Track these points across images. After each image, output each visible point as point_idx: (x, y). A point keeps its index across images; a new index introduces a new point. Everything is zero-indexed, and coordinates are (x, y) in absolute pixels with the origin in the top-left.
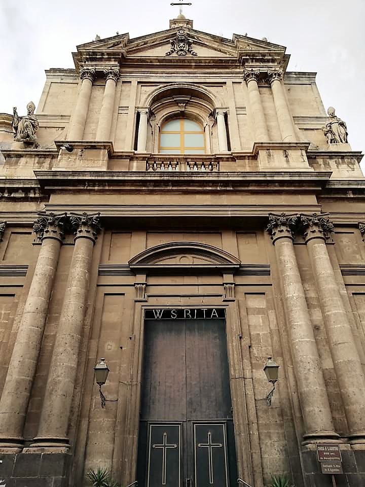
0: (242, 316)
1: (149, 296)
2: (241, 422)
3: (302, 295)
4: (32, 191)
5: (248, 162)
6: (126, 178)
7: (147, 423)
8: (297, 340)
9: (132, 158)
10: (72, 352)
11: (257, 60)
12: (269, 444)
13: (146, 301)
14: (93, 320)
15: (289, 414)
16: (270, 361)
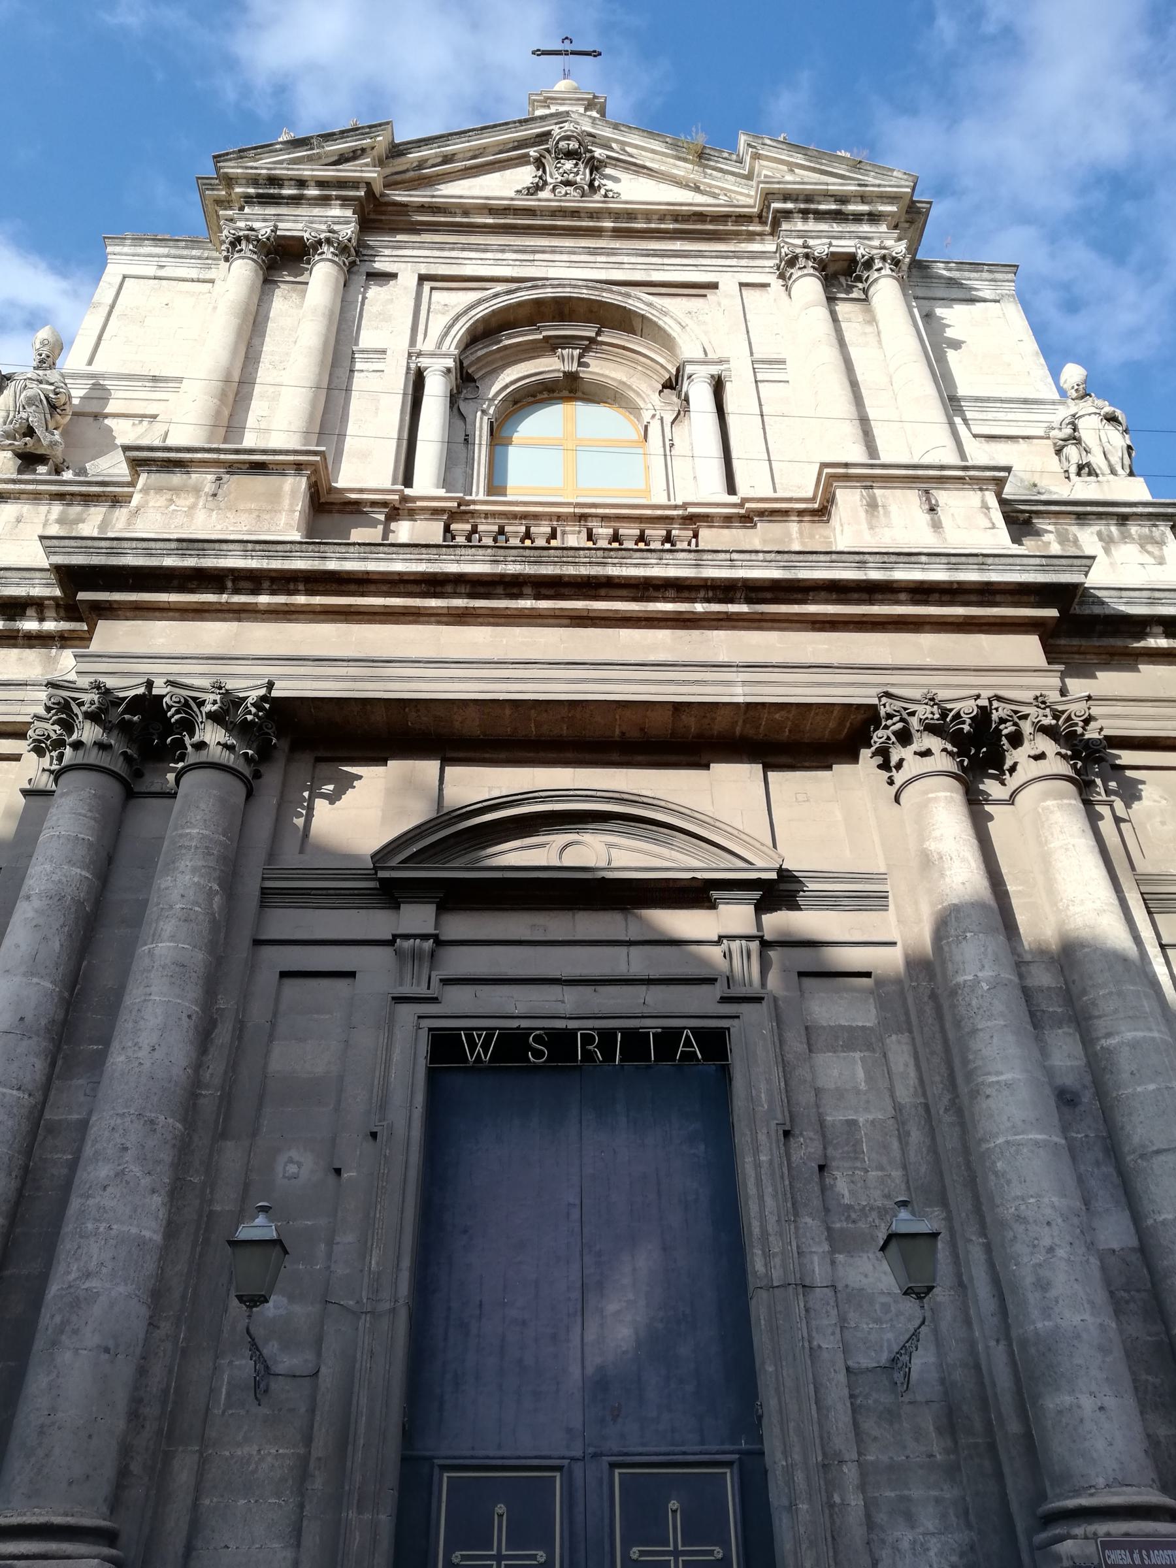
0: (789, 1057)
1: (446, 982)
2: (797, 1457)
3: (1008, 975)
4: (30, 612)
5: (800, 529)
6: (372, 566)
7: (432, 1466)
8: (1000, 1140)
9: (396, 511)
10: (146, 1181)
11: (820, 216)
12: (905, 1545)
13: (434, 1000)
14: (233, 1066)
15: (978, 1425)
16: (904, 1214)
